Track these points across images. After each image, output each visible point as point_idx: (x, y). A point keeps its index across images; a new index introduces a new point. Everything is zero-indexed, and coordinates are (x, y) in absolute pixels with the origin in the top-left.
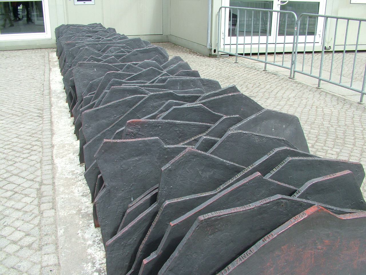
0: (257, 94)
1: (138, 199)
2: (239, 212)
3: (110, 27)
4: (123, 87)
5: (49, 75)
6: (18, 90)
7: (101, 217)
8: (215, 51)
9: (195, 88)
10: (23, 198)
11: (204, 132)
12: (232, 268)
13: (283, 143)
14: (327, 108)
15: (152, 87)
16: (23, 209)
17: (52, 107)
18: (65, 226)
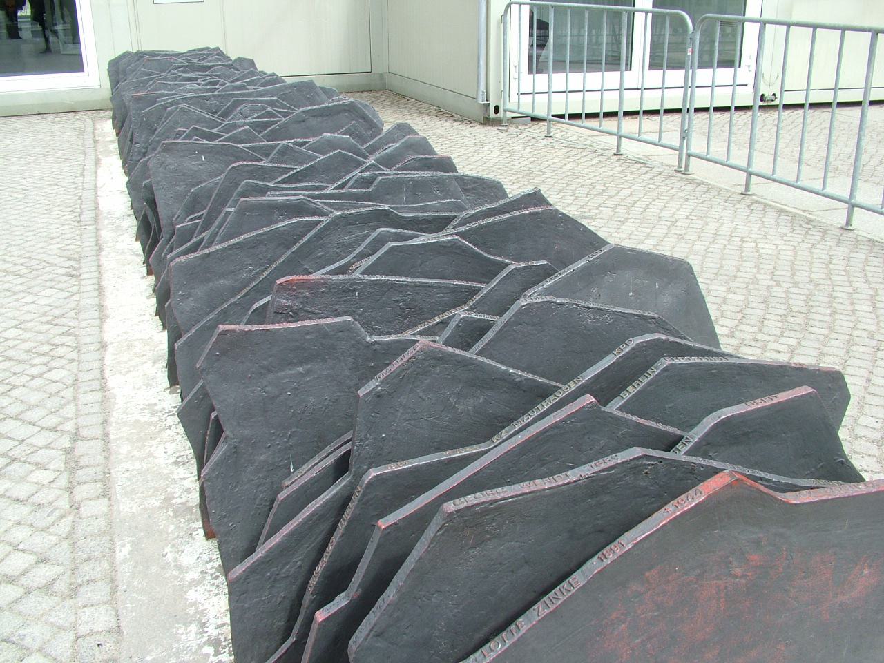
0: (597, 211)
1: (305, 467)
2: (542, 492)
3: (241, 56)
4: (269, 198)
5: (94, 175)
6: (19, 213)
7: (218, 512)
8: (497, 110)
9: (444, 199)
10: (32, 471)
11: (465, 303)
12: (525, 626)
13: (653, 326)
14: (767, 241)
15: (340, 197)
16: (31, 500)
17: (103, 253)
18: (132, 537)
